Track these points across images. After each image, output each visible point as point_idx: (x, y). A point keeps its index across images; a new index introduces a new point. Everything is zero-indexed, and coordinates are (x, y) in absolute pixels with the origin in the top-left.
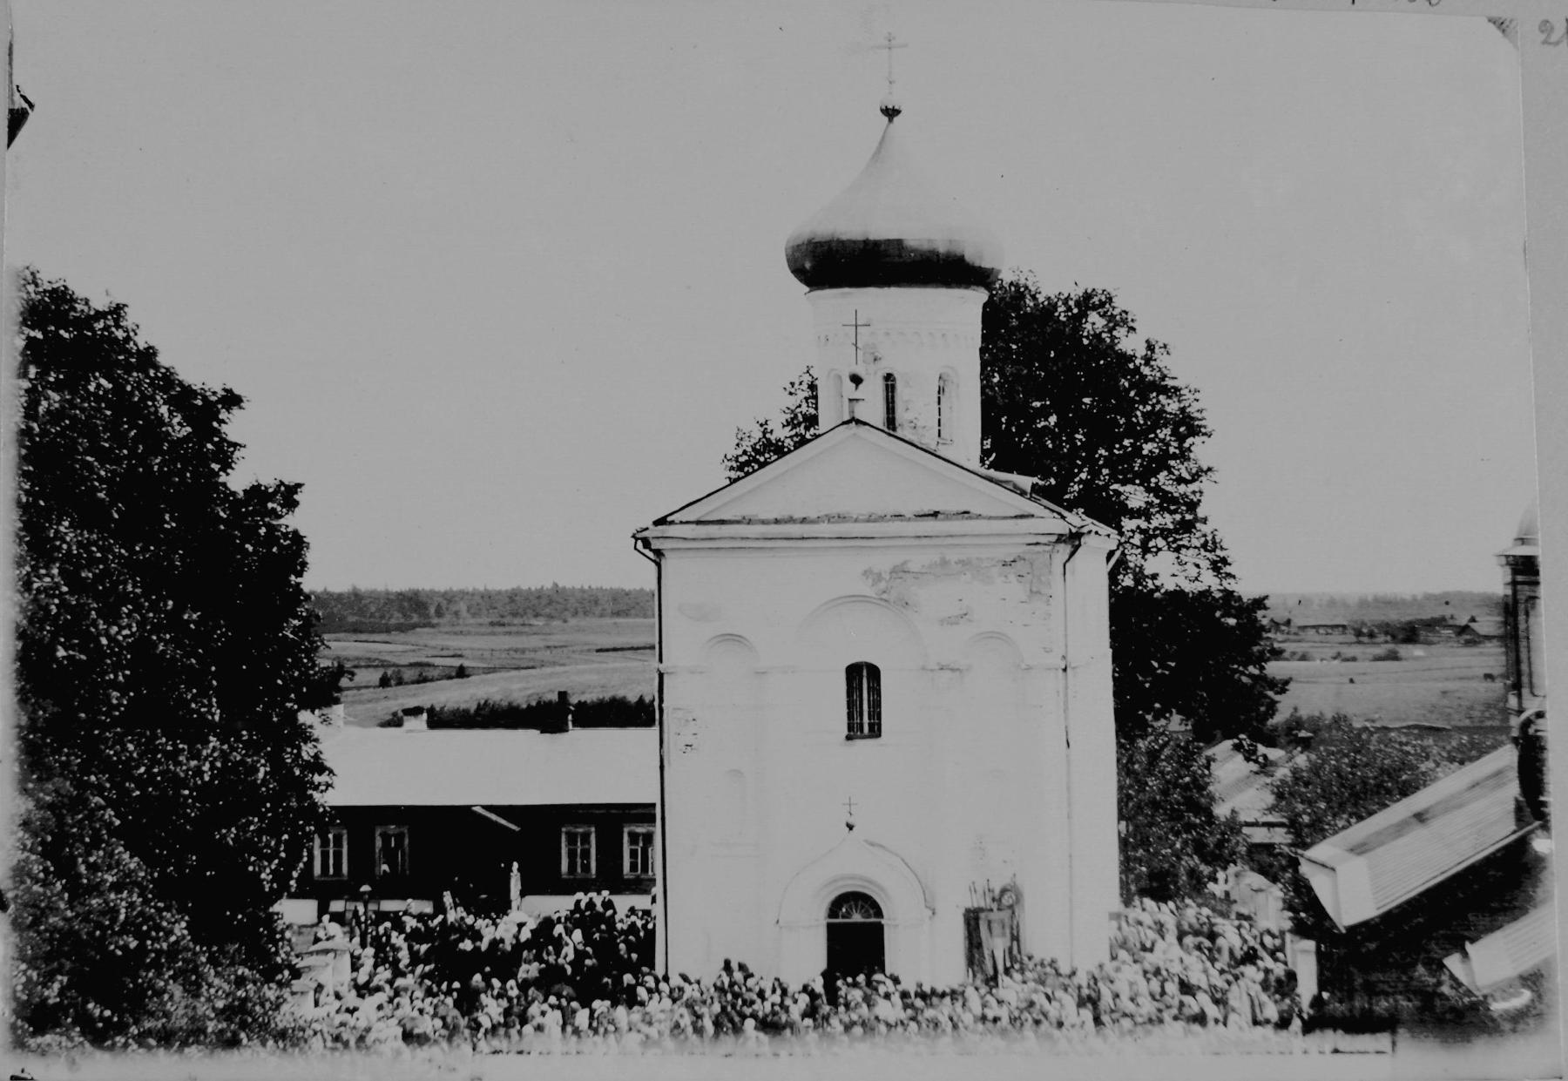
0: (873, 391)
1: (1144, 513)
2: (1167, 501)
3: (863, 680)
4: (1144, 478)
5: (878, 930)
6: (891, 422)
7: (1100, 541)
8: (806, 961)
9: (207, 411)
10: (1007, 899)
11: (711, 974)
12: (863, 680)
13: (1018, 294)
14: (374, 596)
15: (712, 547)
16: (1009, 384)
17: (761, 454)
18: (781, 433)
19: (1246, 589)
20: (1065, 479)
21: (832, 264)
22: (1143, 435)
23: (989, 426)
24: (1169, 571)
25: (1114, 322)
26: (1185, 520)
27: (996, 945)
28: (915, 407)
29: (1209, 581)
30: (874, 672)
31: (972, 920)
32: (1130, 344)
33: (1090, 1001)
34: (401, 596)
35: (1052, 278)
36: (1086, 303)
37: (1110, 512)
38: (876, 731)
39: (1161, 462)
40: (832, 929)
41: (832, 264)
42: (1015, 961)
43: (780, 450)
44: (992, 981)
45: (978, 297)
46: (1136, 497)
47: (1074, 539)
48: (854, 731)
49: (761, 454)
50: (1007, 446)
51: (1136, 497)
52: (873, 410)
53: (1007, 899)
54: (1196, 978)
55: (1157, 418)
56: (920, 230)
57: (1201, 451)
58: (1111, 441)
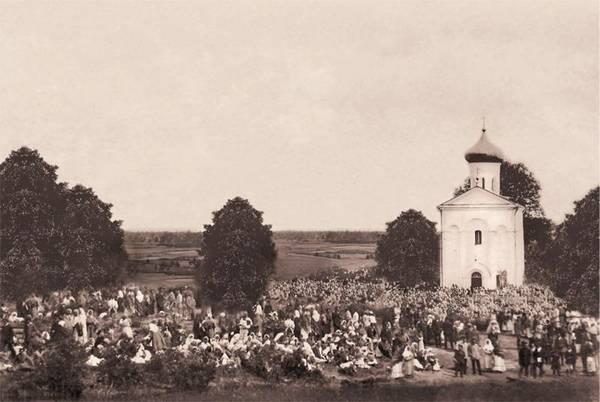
0: (480, 181)
1: (530, 204)
2: (534, 202)
3: (478, 234)
4: (529, 197)
5: (480, 279)
6: (483, 187)
7: (522, 209)
8: (467, 284)
9: (107, 207)
10: (504, 273)
11: (450, 287)
12: (478, 234)
13: (507, 163)
14: (364, 233)
15: (450, 209)
16: (505, 181)
17: (459, 193)
18: (463, 189)
19: (548, 217)
20: (515, 197)
21: (473, 158)
22: (529, 189)
23: (501, 188)
24: (533, 214)
25: (524, 169)
26: (536, 206)
27: (502, 282)
28: (488, 186)
29: (541, 216)
30: (480, 232)
31: (498, 277)
32: (527, 173)
33: (519, 292)
34: (373, 233)
35: (512, 158)
36: (519, 165)
37: (523, 203)
38: (476, 232)
39: (533, 194)
40: (473, 279)
41: (473, 158)
42: (506, 285)
43: (463, 192)
44: (501, 288)
45: (499, 164)
46: (528, 201)
47: (517, 208)
48: (476, 243)
49: (459, 193)
50: (505, 191)
51: (528, 201)
52: (481, 185)
53: (504, 273)
54: (539, 288)
55: (532, 186)
56: (488, 152)
57: (540, 192)
58: (523, 190)
